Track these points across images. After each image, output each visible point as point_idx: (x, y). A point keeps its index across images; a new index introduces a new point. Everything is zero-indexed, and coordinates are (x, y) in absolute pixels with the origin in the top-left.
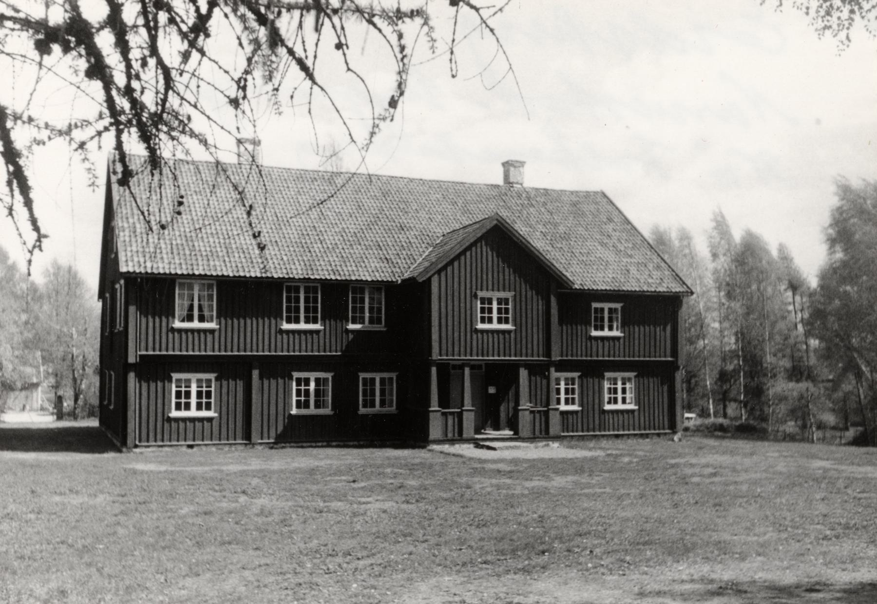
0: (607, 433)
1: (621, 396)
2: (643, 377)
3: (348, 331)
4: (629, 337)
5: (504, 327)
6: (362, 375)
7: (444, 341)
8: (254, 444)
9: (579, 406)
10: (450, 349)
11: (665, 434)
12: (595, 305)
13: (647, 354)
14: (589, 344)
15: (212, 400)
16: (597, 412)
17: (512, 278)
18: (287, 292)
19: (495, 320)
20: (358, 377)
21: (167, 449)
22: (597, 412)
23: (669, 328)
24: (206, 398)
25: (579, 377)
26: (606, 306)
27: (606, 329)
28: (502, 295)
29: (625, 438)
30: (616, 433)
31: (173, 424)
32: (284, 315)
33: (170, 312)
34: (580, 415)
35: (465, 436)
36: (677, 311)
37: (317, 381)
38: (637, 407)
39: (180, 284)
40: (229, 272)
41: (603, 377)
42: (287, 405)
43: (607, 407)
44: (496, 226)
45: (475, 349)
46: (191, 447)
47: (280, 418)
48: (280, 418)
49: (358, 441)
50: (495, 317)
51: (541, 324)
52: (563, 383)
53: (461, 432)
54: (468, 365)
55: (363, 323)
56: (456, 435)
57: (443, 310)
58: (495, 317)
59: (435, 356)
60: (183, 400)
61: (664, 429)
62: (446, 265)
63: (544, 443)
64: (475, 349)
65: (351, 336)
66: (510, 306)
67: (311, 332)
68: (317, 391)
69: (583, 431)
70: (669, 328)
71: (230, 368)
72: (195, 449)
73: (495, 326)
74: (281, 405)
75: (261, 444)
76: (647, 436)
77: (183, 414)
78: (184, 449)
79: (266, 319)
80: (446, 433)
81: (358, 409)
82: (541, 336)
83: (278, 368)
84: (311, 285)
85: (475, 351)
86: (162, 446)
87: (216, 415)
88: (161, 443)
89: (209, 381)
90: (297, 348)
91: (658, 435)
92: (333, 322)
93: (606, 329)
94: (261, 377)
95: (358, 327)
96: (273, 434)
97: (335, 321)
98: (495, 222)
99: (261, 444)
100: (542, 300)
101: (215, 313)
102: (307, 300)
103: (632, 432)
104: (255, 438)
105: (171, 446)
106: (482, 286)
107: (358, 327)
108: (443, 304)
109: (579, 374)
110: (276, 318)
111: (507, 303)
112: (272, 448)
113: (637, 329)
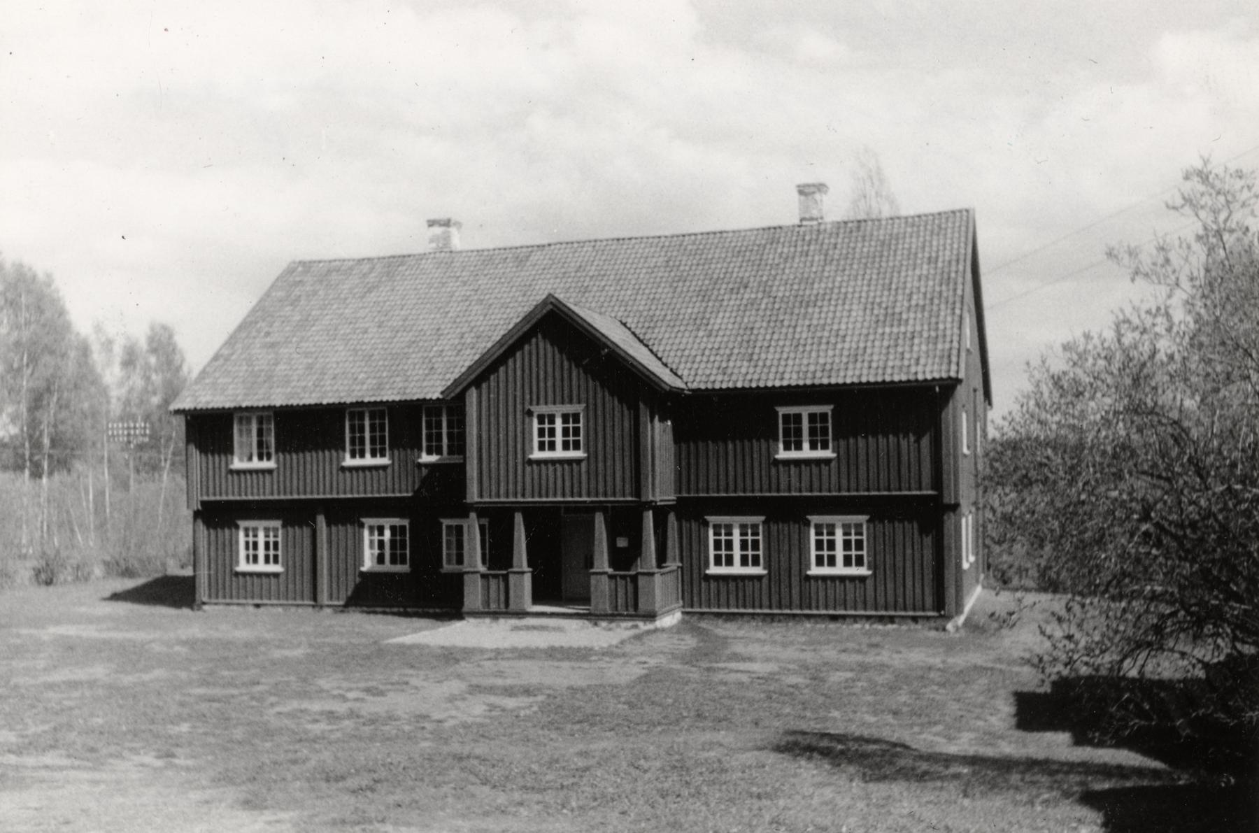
0: (815, 612)
1: (836, 552)
2: (882, 521)
3: (420, 466)
4: (847, 460)
5: (572, 454)
6: (446, 522)
7: (485, 478)
8: (321, 607)
9: (869, 568)
10: (390, 485)
11: (928, 618)
12: (782, 411)
13: (765, 487)
14: (773, 471)
15: (761, 553)
16: (795, 581)
17: (582, 382)
18: (448, 415)
19: (559, 445)
20: (441, 524)
21: (235, 608)
22: (795, 581)
23: (925, 441)
24: (857, 549)
25: (764, 522)
26: (805, 411)
27: (368, 455)
28: (569, 409)
29: (746, 618)
30: (831, 612)
31: (713, 585)
32: (424, 444)
33: (228, 449)
34: (765, 581)
35: (512, 607)
36: (941, 413)
37: (393, 529)
38: (870, 573)
39: (241, 420)
40: (278, 401)
41: (362, 525)
42: (359, 559)
43: (815, 570)
44: (551, 313)
45: (528, 487)
46: (258, 606)
47: (350, 578)
48: (350, 578)
49: (405, 607)
50: (553, 443)
51: (627, 448)
52: (261, 535)
53: (636, 606)
54: (518, 510)
55: (439, 452)
56: (502, 606)
57: (484, 436)
58: (553, 443)
59: (473, 495)
60: (825, 553)
61: (924, 609)
62: (485, 372)
63: (630, 624)
64: (528, 487)
65: (425, 471)
66: (581, 425)
67: (818, 462)
68: (393, 542)
69: (770, 607)
70: (925, 441)
71: (295, 513)
72: (262, 609)
73: (559, 453)
74: (350, 561)
75: (328, 606)
76: (891, 619)
77: (825, 571)
78: (251, 609)
79: (870, 438)
80: (487, 603)
81: (442, 566)
82: (627, 463)
83: (347, 513)
84: (380, 410)
85: (528, 491)
86: (228, 604)
87: (765, 572)
88: (228, 601)
89: (858, 526)
90: (362, 488)
91: (915, 619)
92: (217, 457)
93: (368, 455)
94: (329, 525)
95: (434, 458)
96: (343, 596)
97: (742, 441)
98: (550, 307)
99: (328, 606)
100: (629, 409)
101: (830, 437)
102: (373, 429)
103: (862, 613)
104: (324, 598)
105: (238, 604)
106: (538, 398)
107: (434, 458)
108: (484, 427)
109: (763, 518)
110: (767, 441)
111: (576, 420)
112: (342, 611)
113: (861, 443)
